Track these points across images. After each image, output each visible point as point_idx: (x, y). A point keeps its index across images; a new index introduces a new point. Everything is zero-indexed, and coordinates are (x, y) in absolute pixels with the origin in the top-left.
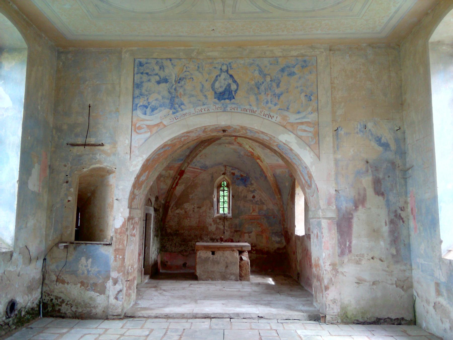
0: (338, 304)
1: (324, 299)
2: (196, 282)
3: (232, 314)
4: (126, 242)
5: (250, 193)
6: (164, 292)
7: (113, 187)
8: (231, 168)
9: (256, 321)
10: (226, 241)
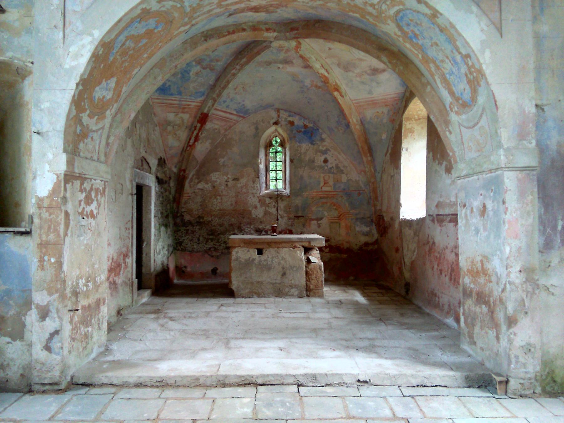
0: (536, 355)
1: (504, 342)
2: (230, 301)
3: (302, 375)
4: (62, 227)
5: (319, 154)
6: (171, 323)
7: (30, 106)
8: (287, 114)
9: (352, 391)
10: (280, 233)
